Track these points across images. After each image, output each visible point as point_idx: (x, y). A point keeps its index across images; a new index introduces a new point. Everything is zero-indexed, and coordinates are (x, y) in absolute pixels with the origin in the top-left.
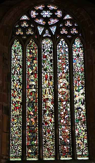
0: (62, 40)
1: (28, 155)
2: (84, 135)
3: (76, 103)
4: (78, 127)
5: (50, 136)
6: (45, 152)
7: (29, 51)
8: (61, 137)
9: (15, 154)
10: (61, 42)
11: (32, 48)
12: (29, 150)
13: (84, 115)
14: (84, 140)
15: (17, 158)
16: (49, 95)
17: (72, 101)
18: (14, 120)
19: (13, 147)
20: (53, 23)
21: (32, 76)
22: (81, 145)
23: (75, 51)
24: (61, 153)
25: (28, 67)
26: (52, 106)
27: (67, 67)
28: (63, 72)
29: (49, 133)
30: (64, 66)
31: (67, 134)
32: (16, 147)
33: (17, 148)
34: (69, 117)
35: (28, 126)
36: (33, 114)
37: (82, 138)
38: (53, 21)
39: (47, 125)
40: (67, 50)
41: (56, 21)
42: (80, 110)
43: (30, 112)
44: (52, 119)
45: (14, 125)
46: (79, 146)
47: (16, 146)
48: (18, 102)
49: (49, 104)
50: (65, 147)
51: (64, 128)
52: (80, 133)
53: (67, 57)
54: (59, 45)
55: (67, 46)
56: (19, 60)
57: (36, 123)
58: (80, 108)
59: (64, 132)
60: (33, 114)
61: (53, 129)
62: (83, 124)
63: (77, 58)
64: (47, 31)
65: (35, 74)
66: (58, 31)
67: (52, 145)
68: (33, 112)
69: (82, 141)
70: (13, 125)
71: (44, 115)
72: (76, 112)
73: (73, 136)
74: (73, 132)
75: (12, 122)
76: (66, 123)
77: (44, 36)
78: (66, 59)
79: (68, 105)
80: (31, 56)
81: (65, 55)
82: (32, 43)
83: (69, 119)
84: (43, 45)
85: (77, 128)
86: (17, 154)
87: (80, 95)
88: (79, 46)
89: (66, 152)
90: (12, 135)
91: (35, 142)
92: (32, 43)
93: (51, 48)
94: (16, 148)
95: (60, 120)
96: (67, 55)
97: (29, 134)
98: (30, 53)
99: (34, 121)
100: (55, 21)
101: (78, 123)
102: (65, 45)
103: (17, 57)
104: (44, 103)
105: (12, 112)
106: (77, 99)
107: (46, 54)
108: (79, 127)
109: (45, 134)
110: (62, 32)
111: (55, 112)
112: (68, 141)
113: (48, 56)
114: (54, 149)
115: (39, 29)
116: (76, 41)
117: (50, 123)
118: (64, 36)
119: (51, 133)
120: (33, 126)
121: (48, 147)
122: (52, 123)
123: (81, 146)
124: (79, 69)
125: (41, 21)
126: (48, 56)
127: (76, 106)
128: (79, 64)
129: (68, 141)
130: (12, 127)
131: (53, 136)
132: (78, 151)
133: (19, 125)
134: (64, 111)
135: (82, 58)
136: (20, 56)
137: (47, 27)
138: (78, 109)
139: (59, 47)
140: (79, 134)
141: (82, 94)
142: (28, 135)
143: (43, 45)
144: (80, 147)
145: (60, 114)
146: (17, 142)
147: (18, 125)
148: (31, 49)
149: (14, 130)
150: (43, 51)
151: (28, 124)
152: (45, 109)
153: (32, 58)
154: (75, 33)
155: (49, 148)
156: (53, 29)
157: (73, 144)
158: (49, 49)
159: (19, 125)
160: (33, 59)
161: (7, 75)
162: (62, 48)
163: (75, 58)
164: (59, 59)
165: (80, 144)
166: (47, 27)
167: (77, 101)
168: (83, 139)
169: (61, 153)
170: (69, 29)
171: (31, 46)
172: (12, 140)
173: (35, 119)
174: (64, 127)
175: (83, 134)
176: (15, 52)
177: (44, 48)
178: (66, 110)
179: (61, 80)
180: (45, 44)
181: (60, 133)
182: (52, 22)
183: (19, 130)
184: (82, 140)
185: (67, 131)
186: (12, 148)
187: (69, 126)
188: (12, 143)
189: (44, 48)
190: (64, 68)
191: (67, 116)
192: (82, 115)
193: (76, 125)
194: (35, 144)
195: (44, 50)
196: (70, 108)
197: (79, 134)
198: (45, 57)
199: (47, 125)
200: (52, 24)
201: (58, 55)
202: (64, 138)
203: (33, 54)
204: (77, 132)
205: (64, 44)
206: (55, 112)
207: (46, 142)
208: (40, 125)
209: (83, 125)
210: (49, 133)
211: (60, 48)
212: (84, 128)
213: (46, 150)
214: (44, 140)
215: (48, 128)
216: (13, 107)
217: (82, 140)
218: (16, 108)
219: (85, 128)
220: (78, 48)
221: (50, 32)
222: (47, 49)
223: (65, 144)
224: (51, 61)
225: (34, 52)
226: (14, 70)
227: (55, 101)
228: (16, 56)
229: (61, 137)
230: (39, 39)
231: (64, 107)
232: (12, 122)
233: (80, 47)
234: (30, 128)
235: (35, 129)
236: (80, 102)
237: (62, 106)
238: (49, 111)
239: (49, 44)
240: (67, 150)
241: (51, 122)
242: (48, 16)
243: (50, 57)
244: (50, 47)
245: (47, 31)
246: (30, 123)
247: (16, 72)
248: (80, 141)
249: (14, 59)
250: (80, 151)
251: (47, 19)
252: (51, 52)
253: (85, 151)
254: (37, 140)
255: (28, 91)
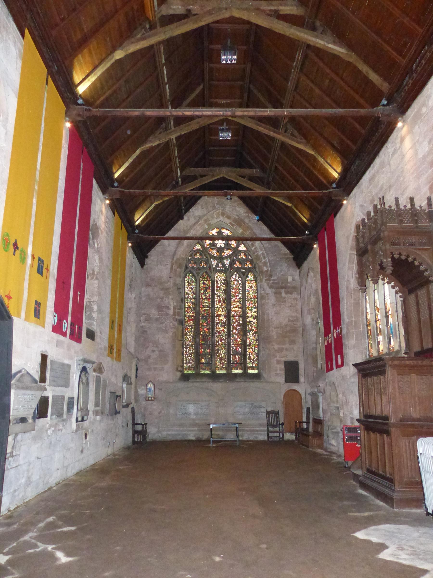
0: (236, 273)
1: (201, 366)
2: (255, 344)
3: (249, 317)
4: (250, 336)
5: (223, 344)
6: (218, 362)
7: (202, 282)
8: (233, 346)
9: (189, 364)
10: (234, 275)
11: (205, 279)
12: (203, 359)
13: (256, 327)
14: (254, 349)
15: (191, 370)
16: (222, 312)
17: (244, 316)
18: (187, 329)
19: (186, 355)
20: (227, 254)
21: (206, 300)
22: (252, 354)
23: (249, 284)
24: (233, 363)
25: (202, 294)
26: (224, 320)
27: (240, 295)
28: (237, 298)
29: (221, 341)
30: (237, 294)
31: (239, 343)
32: (189, 356)
33: (191, 357)
34: (241, 328)
35: (201, 335)
36: (206, 325)
37: (253, 347)
38: (227, 252)
39: (220, 334)
40: (240, 282)
41: (230, 252)
42: (252, 323)
43: (203, 323)
44: (225, 329)
45: (188, 334)
46: (250, 355)
47: (190, 354)
48: (192, 316)
49: (222, 318)
50: (237, 357)
51: (236, 337)
52: (251, 343)
53: (240, 288)
54: (233, 278)
55: (240, 279)
56: (193, 289)
57: (209, 332)
58: (252, 322)
59: (236, 341)
60: (206, 325)
61: (225, 338)
62: (255, 334)
63: (250, 289)
64: (220, 265)
65: (209, 299)
66: (232, 264)
67: (224, 354)
68: (207, 323)
69: (252, 350)
70: (187, 333)
71: (217, 326)
72: (248, 325)
73: (244, 345)
74: (244, 342)
75: (186, 331)
76: (238, 333)
77: (218, 269)
78: (239, 289)
79: (241, 319)
80: (205, 286)
81: (238, 286)
82: (205, 275)
83: (241, 330)
84: (217, 277)
85: (248, 337)
86: (191, 364)
87: (252, 312)
88: (252, 279)
89: (238, 363)
90: (186, 342)
91: (208, 351)
92: (205, 275)
93: (224, 280)
94: (190, 357)
95: (232, 330)
96: (240, 286)
97: (203, 342)
98: (204, 283)
99: (207, 331)
100: (229, 252)
101: (250, 333)
102: (238, 278)
103: (190, 286)
104: (217, 317)
105: (186, 322)
106: (250, 315)
107: (219, 285)
108: (251, 337)
109: (218, 342)
110: (236, 266)
111: (228, 324)
112: (240, 350)
113: (221, 286)
114: (226, 358)
115: (213, 261)
116: (249, 274)
117: (223, 333)
118: (238, 270)
119: (223, 342)
120: (206, 335)
121: (220, 356)
122: (224, 333)
123: (252, 356)
124: (252, 296)
125: (214, 252)
126: (221, 286)
127: (248, 320)
128: (252, 293)
129: (240, 350)
130: (186, 335)
131: (225, 344)
132: (248, 361)
133: (193, 333)
134: (237, 323)
135: (255, 289)
136: (193, 286)
137: (221, 259)
138: (250, 322)
139: (233, 279)
140: (250, 343)
141: (255, 312)
142: (201, 343)
143: (217, 277)
144: (251, 357)
145: (232, 325)
146: (190, 350)
147: (192, 333)
148: (205, 280)
149: (188, 338)
150: (217, 283)
151: (201, 333)
152: (218, 321)
153: (205, 287)
154: (248, 267)
155: (221, 358)
156: (227, 262)
157: (244, 354)
158: (223, 281)
159: (193, 333)
160: (206, 288)
161: (196, 226)
162: (235, 280)
163: (248, 288)
164: (232, 289)
165: (251, 353)
166: (221, 259)
167: (249, 316)
168: (254, 348)
169: (233, 363)
170: (242, 262)
171: (204, 278)
172: (186, 348)
173: (209, 329)
174: (235, 336)
175: (255, 343)
176: (188, 282)
177: (218, 280)
178: (239, 323)
179: (234, 303)
180: (219, 277)
181: (232, 342)
182: (226, 254)
183: (193, 338)
184: (253, 349)
185: (239, 340)
186: (186, 356)
187: (241, 335)
188: (186, 351)
189: (218, 280)
190: (237, 296)
191: (239, 327)
192: (254, 327)
193: (248, 335)
194: (208, 352)
195: (217, 282)
196: (242, 321)
197: (250, 343)
198: (219, 287)
199: (220, 334)
200: (226, 255)
201: (232, 286)
202: (235, 347)
203: (206, 284)
204: (248, 341)
205: (237, 277)
206: (228, 324)
207: (218, 350)
208: (213, 334)
209: (254, 335)
210: (221, 341)
211: (233, 280)
212: (255, 337)
213: (219, 360)
214: (216, 348)
215: (220, 337)
216: (186, 319)
217: (253, 349)
218: (189, 320)
219: (256, 338)
220: (251, 281)
221: (224, 265)
222: (220, 281)
223: (237, 353)
224: (224, 290)
225: (207, 283)
226: (187, 296)
227: (228, 316)
228: (189, 286)
229: (233, 346)
230: (212, 270)
231: (236, 322)
232: (186, 331)
233: (254, 280)
234: (203, 337)
235: (208, 337)
236: (252, 318)
237: (235, 320)
238: (222, 323)
239: (222, 277)
240: (238, 360)
241: (223, 332)
242: (223, 246)
243: (223, 288)
244: (224, 279)
245: (220, 265)
246: (203, 332)
247: (189, 297)
248: (251, 350)
249: (187, 288)
250: (251, 361)
251: (220, 250)
252: (224, 284)
253: (255, 361)
254: (210, 349)
255: (201, 309)
